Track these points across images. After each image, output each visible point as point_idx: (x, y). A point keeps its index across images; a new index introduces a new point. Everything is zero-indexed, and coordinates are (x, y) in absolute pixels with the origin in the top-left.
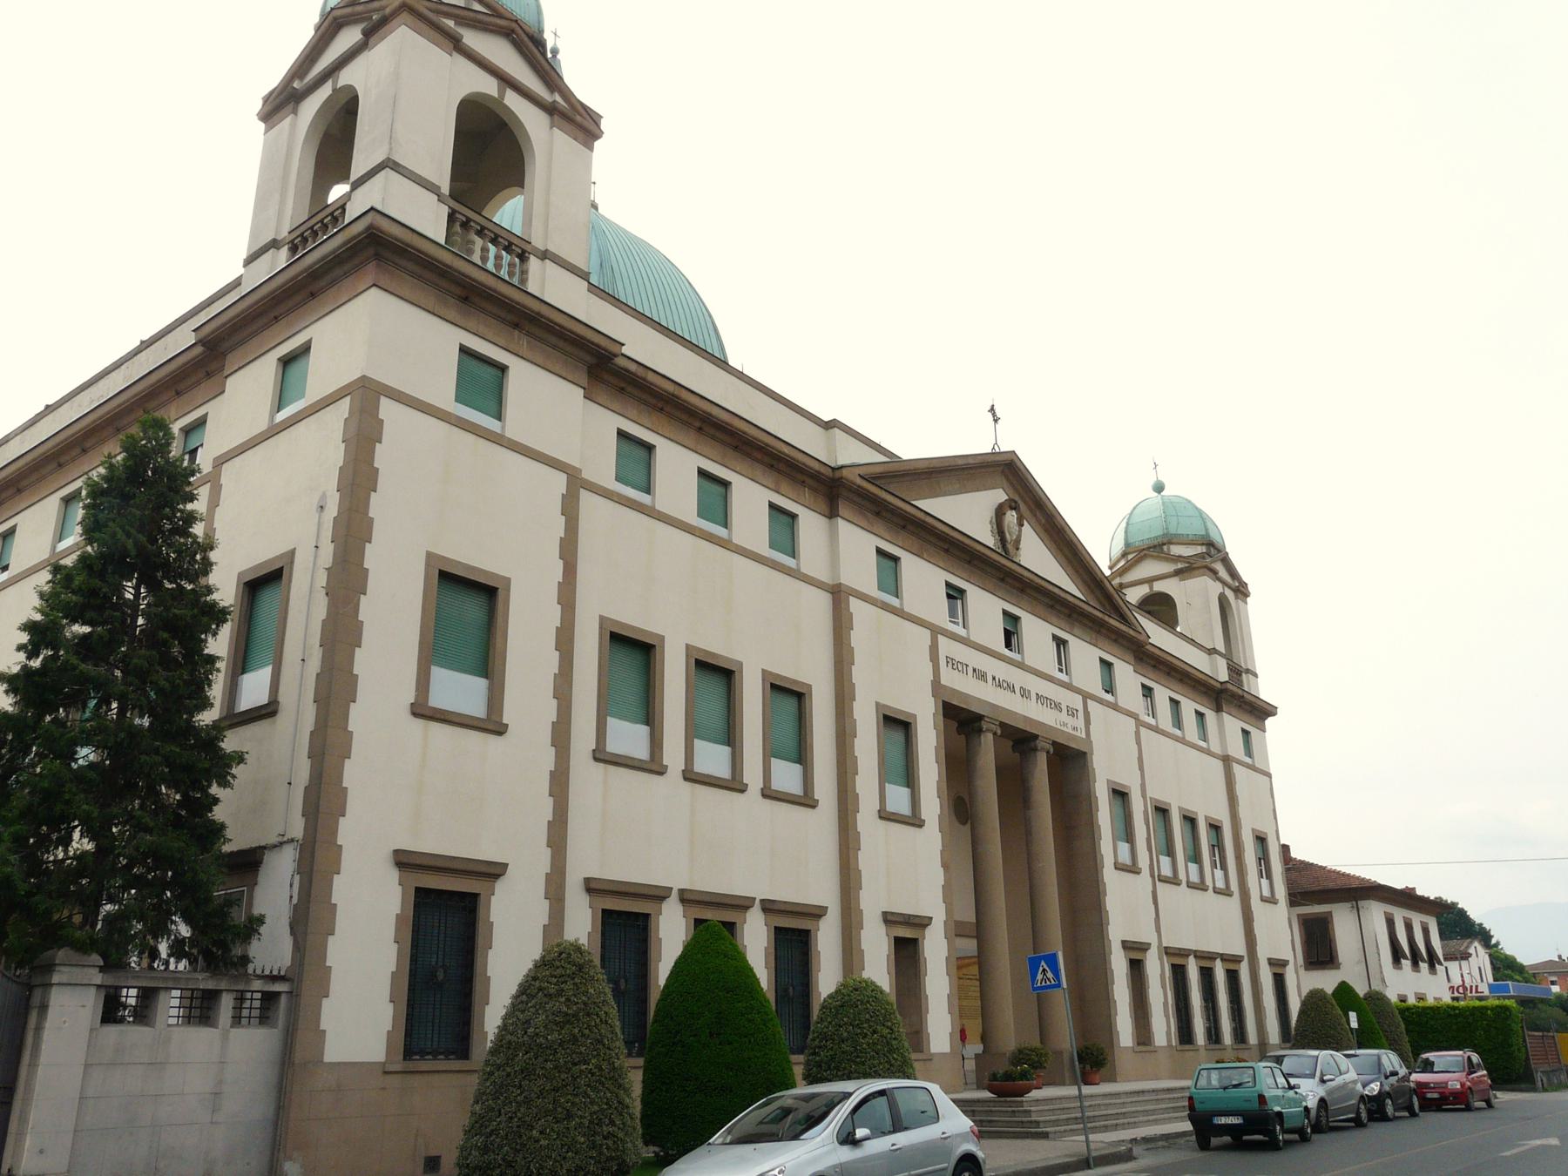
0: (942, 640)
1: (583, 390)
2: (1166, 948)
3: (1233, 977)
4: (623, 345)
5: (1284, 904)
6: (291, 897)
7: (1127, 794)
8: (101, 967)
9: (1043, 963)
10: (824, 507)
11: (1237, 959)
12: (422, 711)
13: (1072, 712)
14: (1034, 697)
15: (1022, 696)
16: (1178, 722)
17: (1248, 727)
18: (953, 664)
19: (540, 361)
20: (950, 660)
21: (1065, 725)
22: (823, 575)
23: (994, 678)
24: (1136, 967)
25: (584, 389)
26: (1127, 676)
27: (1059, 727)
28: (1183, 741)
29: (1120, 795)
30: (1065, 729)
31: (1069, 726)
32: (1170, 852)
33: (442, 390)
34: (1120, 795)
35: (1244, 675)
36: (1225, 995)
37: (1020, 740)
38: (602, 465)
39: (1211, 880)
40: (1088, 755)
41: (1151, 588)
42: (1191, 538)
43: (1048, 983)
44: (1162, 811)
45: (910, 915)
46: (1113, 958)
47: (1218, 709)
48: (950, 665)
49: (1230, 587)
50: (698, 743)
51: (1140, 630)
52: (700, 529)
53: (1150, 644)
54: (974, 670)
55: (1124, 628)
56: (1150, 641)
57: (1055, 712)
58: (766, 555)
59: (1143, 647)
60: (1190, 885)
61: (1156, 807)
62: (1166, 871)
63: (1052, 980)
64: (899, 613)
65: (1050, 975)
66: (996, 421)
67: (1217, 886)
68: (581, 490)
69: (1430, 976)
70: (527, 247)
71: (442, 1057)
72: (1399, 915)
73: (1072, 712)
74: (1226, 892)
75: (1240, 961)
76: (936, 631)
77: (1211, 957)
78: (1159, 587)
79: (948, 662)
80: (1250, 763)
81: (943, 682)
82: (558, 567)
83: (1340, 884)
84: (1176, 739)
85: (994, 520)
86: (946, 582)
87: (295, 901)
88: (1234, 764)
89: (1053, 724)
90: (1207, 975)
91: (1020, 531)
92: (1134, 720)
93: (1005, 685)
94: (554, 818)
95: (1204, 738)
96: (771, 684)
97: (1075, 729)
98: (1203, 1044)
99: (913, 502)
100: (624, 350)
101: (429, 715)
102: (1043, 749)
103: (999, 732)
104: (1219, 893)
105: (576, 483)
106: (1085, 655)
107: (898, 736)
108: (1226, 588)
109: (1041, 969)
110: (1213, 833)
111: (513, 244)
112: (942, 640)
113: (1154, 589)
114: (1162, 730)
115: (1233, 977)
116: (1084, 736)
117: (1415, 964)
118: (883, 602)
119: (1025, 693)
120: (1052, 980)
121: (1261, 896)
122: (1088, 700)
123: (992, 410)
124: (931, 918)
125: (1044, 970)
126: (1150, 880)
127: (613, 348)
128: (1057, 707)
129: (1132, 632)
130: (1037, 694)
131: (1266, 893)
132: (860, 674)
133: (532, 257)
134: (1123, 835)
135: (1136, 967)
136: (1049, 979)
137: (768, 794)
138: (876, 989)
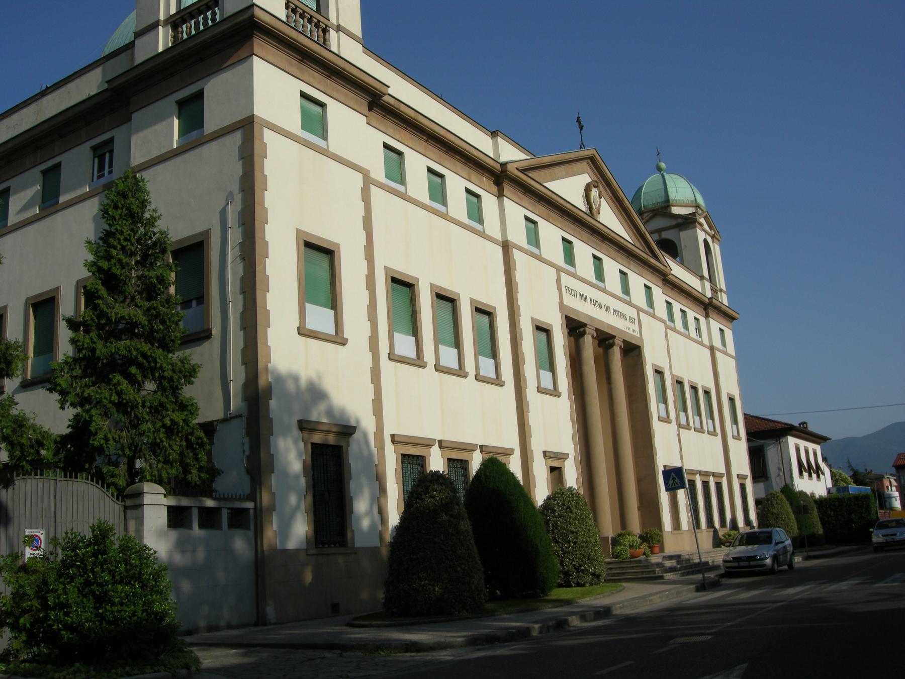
0: (562, 275)
1: (365, 118)
3: (719, 486)
4: (389, 87)
5: (744, 441)
6: (244, 451)
7: (662, 372)
8: (164, 494)
9: (673, 474)
10: (495, 189)
11: (720, 476)
12: (303, 332)
13: (632, 320)
14: (612, 311)
15: (606, 311)
16: (686, 326)
17: (723, 327)
18: (569, 291)
19: (352, 104)
20: (567, 288)
21: (629, 329)
22: (498, 236)
23: (591, 300)
25: (366, 117)
26: (660, 295)
27: (625, 330)
28: (688, 337)
29: (659, 372)
30: (629, 331)
31: (631, 329)
32: (685, 410)
33: (293, 123)
34: (659, 372)
36: (702, 498)
37: (605, 340)
38: (378, 169)
39: (706, 427)
40: (642, 348)
41: (660, 236)
42: (685, 202)
43: (676, 486)
44: (680, 383)
45: (558, 453)
47: (707, 316)
48: (568, 291)
49: (709, 235)
50: (441, 347)
51: (666, 265)
52: (432, 207)
53: (672, 274)
54: (580, 295)
55: (657, 264)
56: (672, 272)
57: (623, 321)
58: (467, 223)
59: (667, 276)
61: (691, 385)
62: (683, 422)
63: (679, 484)
64: (539, 258)
65: (677, 481)
66: (581, 128)
67: (709, 430)
68: (371, 185)
69: (817, 482)
70: (329, 24)
71: (327, 546)
72: (803, 444)
73: (632, 320)
74: (714, 433)
75: (723, 477)
76: (559, 270)
79: (566, 290)
81: (565, 303)
82: (363, 234)
83: (770, 426)
84: (532, 255)
85: (584, 195)
86: (562, 237)
87: (247, 453)
88: (716, 351)
89: (623, 329)
90: (706, 485)
91: (600, 201)
92: (664, 324)
93: (597, 304)
94: (375, 398)
95: (700, 336)
97: (634, 331)
98: (705, 528)
99: (543, 184)
100: (390, 91)
101: (307, 334)
102: (618, 345)
103: (595, 335)
105: (368, 181)
106: (637, 281)
107: (543, 336)
109: (672, 477)
110: (658, 377)
111: (328, 26)
112: (562, 275)
114: (678, 331)
115: (719, 486)
116: (638, 336)
117: (810, 475)
118: (531, 252)
119: (607, 309)
120: (679, 484)
121: (733, 436)
122: (640, 312)
123: (578, 120)
124: (568, 454)
125: (674, 478)
127: (383, 89)
128: (624, 317)
129: (662, 267)
130: (613, 309)
131: (664, 415)
132: (522, 299)
133: (331, 30)
134: (662, 400)
136: (677, 483)
137: (478, 378)
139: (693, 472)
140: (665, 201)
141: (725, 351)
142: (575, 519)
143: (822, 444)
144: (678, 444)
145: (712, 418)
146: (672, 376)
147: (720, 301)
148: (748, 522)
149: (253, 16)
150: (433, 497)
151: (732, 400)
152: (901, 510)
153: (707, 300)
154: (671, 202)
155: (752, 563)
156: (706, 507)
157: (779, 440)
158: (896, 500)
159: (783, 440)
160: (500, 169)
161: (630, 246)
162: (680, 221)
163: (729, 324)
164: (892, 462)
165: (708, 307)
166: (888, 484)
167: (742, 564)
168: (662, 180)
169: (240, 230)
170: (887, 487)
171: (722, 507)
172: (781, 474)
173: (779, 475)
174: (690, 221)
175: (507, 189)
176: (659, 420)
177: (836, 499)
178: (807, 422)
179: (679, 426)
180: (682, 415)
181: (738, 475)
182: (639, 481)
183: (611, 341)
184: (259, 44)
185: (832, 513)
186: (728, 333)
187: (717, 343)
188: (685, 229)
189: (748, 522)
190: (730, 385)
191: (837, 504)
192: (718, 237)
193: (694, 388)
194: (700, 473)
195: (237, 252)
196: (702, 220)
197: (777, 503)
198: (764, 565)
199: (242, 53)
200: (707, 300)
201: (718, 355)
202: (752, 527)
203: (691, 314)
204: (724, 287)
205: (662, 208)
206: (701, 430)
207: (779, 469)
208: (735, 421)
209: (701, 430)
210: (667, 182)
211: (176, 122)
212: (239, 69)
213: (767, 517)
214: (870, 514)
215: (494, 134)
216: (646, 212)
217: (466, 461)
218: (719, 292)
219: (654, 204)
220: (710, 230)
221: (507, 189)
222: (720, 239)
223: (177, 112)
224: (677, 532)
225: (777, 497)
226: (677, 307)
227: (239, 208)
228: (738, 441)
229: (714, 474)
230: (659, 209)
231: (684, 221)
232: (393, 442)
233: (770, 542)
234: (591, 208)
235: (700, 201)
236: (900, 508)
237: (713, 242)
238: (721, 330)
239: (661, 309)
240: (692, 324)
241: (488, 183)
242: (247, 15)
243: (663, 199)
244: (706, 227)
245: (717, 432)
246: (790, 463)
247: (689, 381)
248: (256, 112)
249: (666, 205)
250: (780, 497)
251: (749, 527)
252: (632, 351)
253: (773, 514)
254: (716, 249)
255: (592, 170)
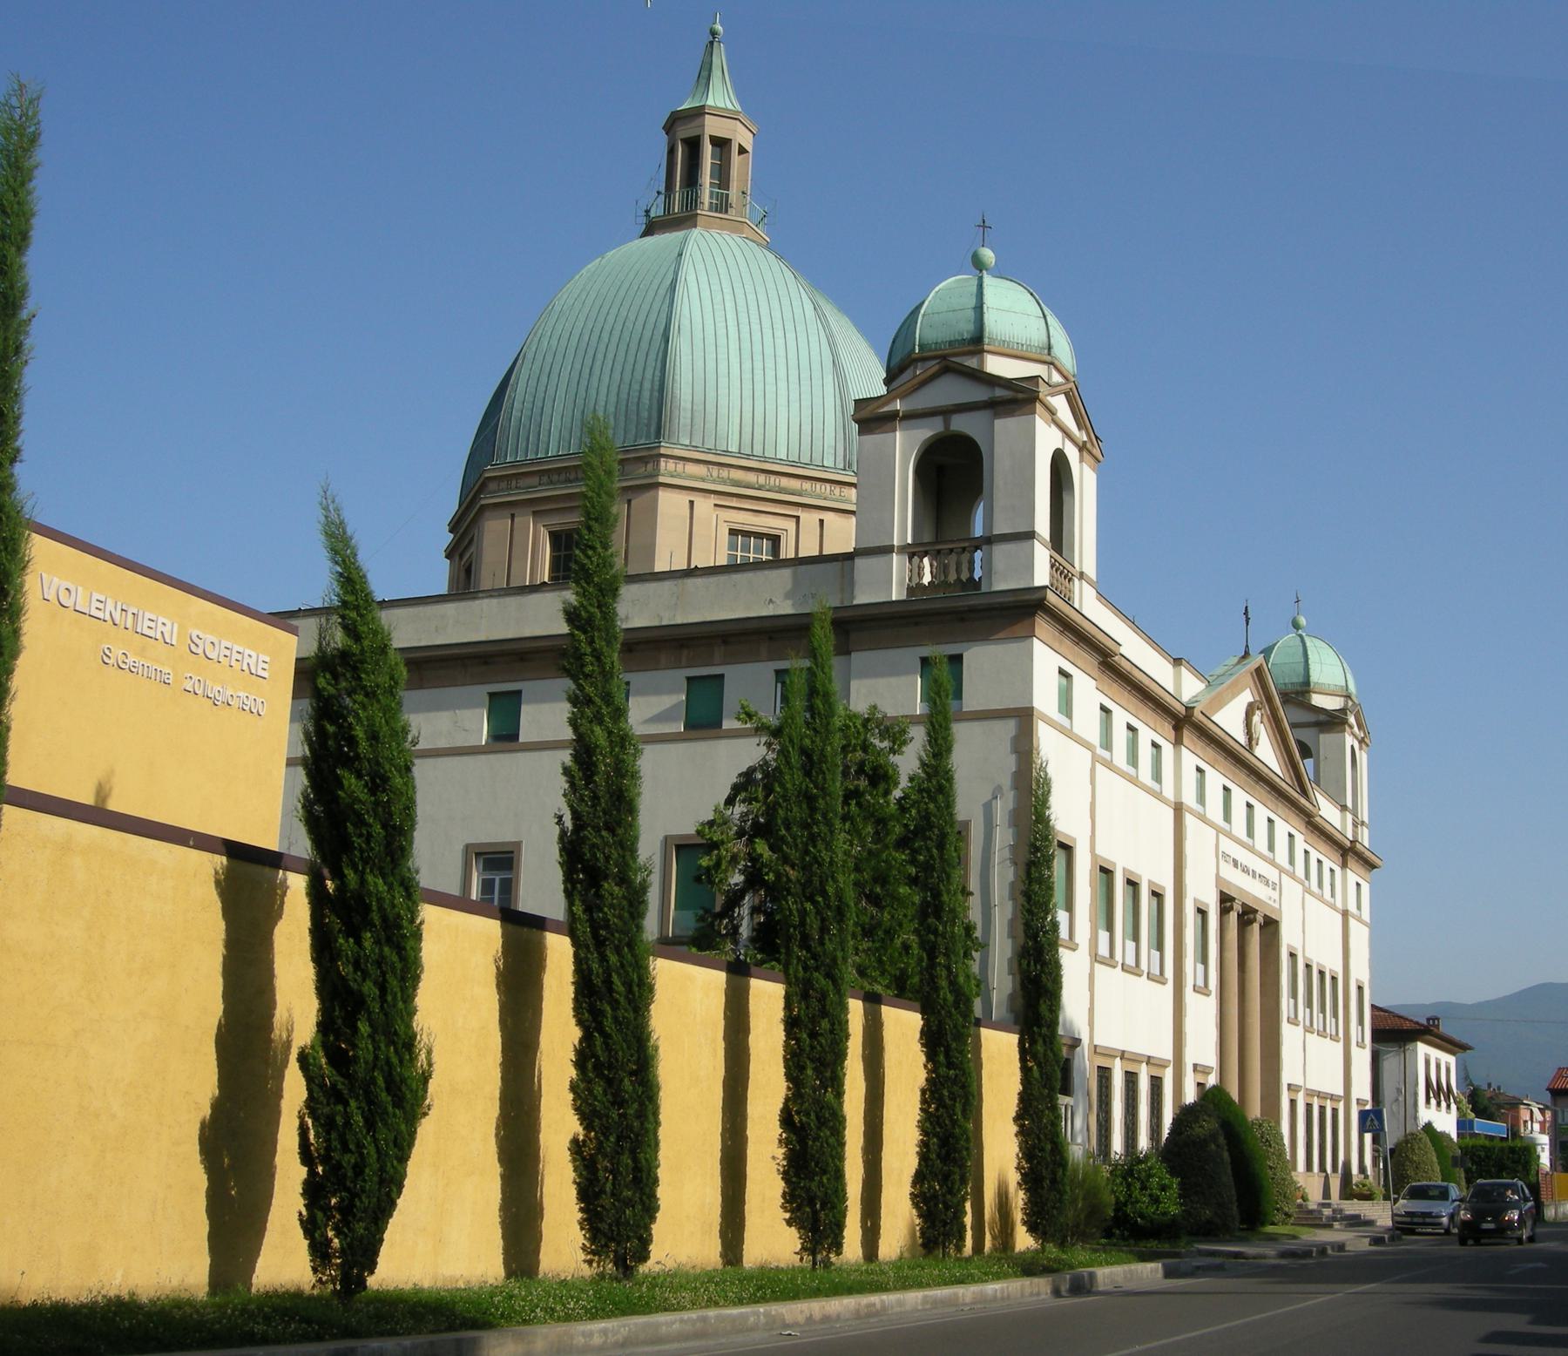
2: (1096, 1046)
3: (1156, 1083)
11: (1162, 1065)
16: (1133, 759)
24: (1293, 1103)
28: (1134, 781)
29: (1292, 955)
32: (1110, 927)
35: (1076, 581)
41: (947, 424)
42: (1332, 688)
44: (1106, 872)
46: (1187, 1079)
51: (1315, 803)
56: (1320, 813)
59: (1313, 817)
60: (1124, 968)
62: (1103, 950)
65: (1376, 1123)
67: (1152, 971)
72: (1435, 1053)
74: (1334, 1038)
75: (1166, 1067)
76: (1219, 830)
77: (1136, 1059)
78: (961, 424)
80: (1202, 812)
81: (1221, 875)
83: (1396, 1024)
90: (1131, 1079)
92: (1301, 887)
96: (1101, 867)
100: (1123, 650)
104: (1198, 992)
108: (1068, 443)
110: (1155, 901)
113: (952, 428)
115: (1156, 1083)
117: (1439, 1104)
121: (1194, 986)
126: (1087, 960)
129: (1310, 807)
131: (1200, 983)
135: (1293, 1103)
138: (1448, 1136)
139: (1109, 1054)
140: (971, 339)
141: (1109, 759)
142: (1273, 1154)
143: (1458, 1055)
144: (1088, 994)
145: (1160, 947)
146: (1304, 956)
147: (1076, 605)
148: (1362, 1169)
149: (1045, 599)
150: (1202, 1127)
151: (1360, 988)
152: (1548, 1170)
153: (1348, 844)
154: (1312, 684)
155: (1428, 1220)
156: (1151, 1125)
157: (1405, 1045)
158: (1543, 1149)
159: (1410, 1046)
160: (1184, 712)
161: (1278, 780)
162: (1322, 717)
163: (1367, 876)
164: (1546, 1085)
165: (1347, 852)
166: (1528, 1118)
167: (1416, 1220)
168: (1301, 648)
169: (1011, 830)
170: (1526, 1122)
171: (1133, 1124)
172: (1401, 1099)
173: (1397, 1100)
174: (1336, 721)
175: (1187, 735)
176: (1194, 990)
177: (1482, 1146)
178: (1439, 1016)
179: (1095, 958)
180: (1103, 936)
181: (1358, 1100)
182: (1345, 1118)
183: (1252, 916)
184: (1042, 625)
185: (1475, 1167)
186: (1365, 887)
187: (1189, 798)
188: (1011, 414)
189: (1362, 1169)
190: (1361, 971)
191: (1483, 1154)
192: (1096, 452)
193: (1132, 884)
194: (1123, 1055)
195: (1007, 853)
196: (1060, 403)
197: (1419, 1148)
198: (1440, 1224)
199: (1019, 629)
200: (1348, 844)
201: (1189, 820)
202: (1366, 1177)
203: (1146, 735)
204: (1090, 569)
205: (1297, 693)
206: (1136, 971)
207: (1399, 1090)
208: (1361, 1022)
209: (1136, 971)
210: (1309, 653)
211: (919, 680)
212: (1013, 647)
213: (1403, 1165)
214: (1528, 1174)
215: (1177, 662)
216: (924, 359)
217: (1136, 1074)
218: (1076, 581)
219: (1285, 684)
220: (1079, 429)
221: (1351, 862)
222: (1100, 457)
223: (920, 670)
224: (1309, 1174)
225: (1420, 1139)
226: (1121, 717)
227: (1011, 806)
228: (1203, 997)
229: (1149, 1060)
230: (1292, 693)
231: (1328, 719)
232: (1358, 1103)
233: (1447, 1199)
234: (1250, 739)
235: (1063, 350)
236: (1548, 1165)
237: (1361, 749)
238: (1226, 789)
239: (1087, 720)
240: (1145, 752)
241: (1337, 857)
242: (1037, 596)
243: (1301, 680)
244: (1356, 729)
245: (1117, 959)
246: (1417, 1084)
247: (1149, 881)
248: (1036, 704)
249: (1304, 688)
250: (1423, 1141)
251: (1363, 1176)
252: (1271, 926)
253: (1412, 1161)
254: (1085, 479)
255: (1255, 683)
